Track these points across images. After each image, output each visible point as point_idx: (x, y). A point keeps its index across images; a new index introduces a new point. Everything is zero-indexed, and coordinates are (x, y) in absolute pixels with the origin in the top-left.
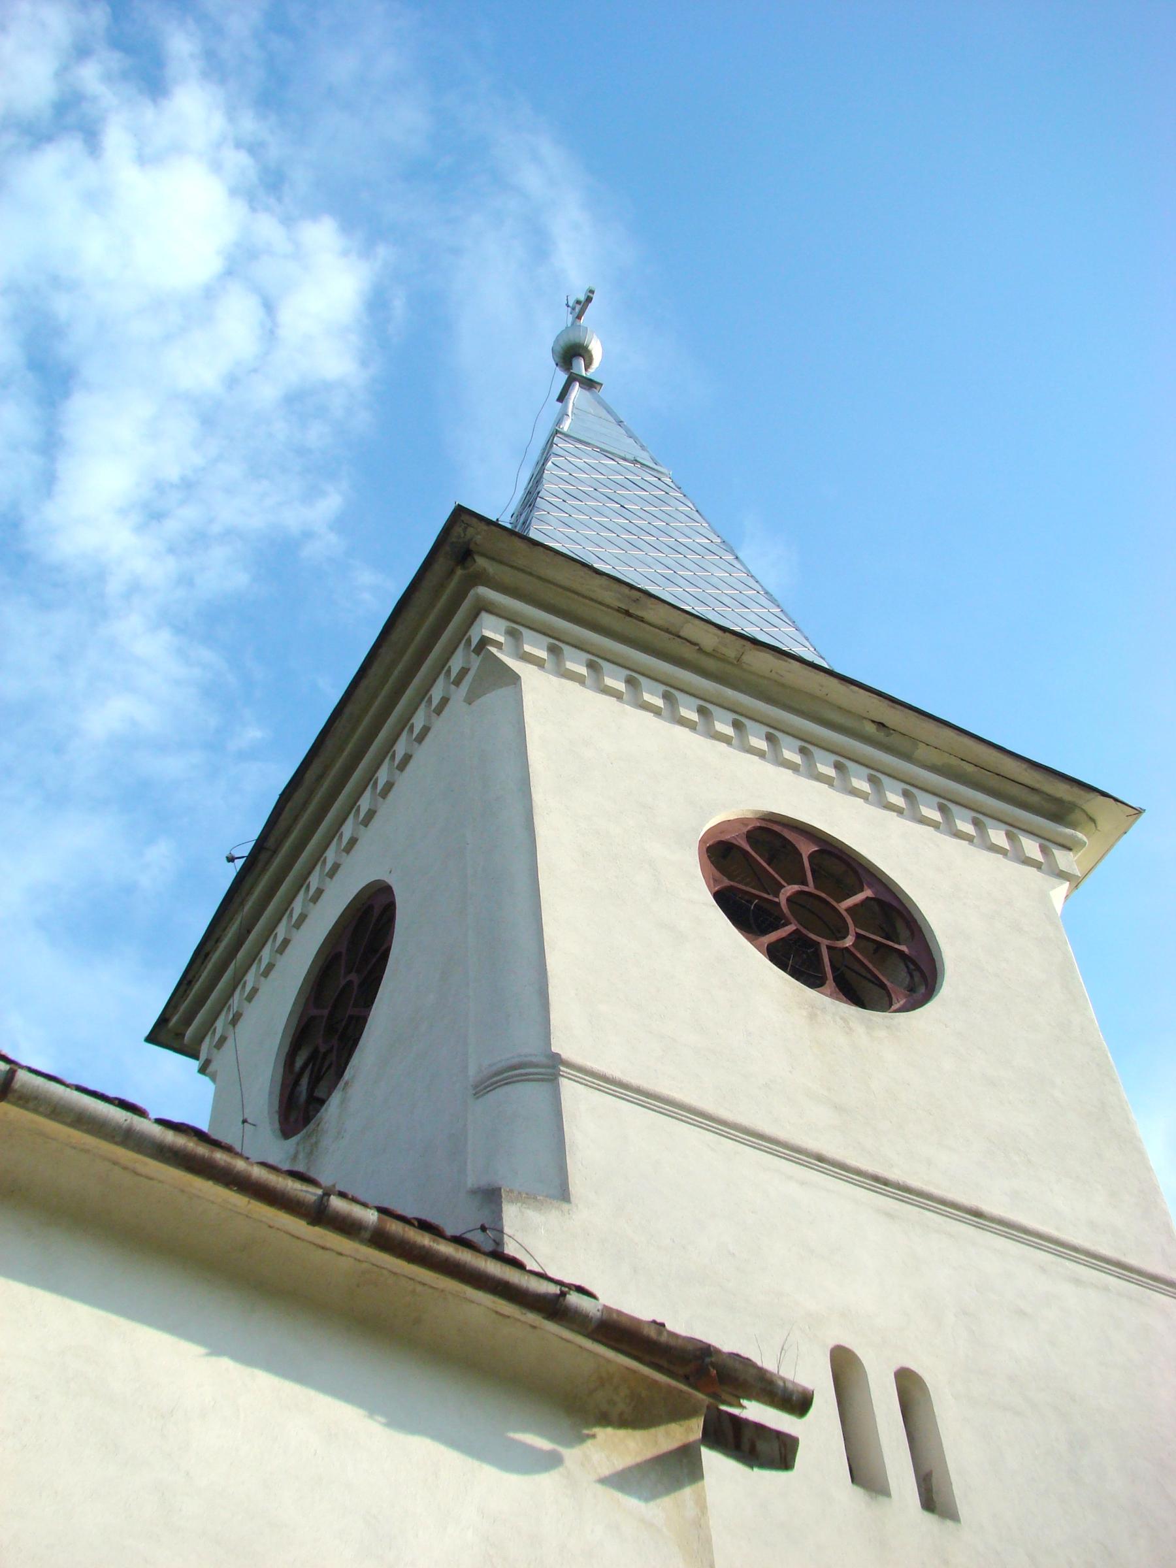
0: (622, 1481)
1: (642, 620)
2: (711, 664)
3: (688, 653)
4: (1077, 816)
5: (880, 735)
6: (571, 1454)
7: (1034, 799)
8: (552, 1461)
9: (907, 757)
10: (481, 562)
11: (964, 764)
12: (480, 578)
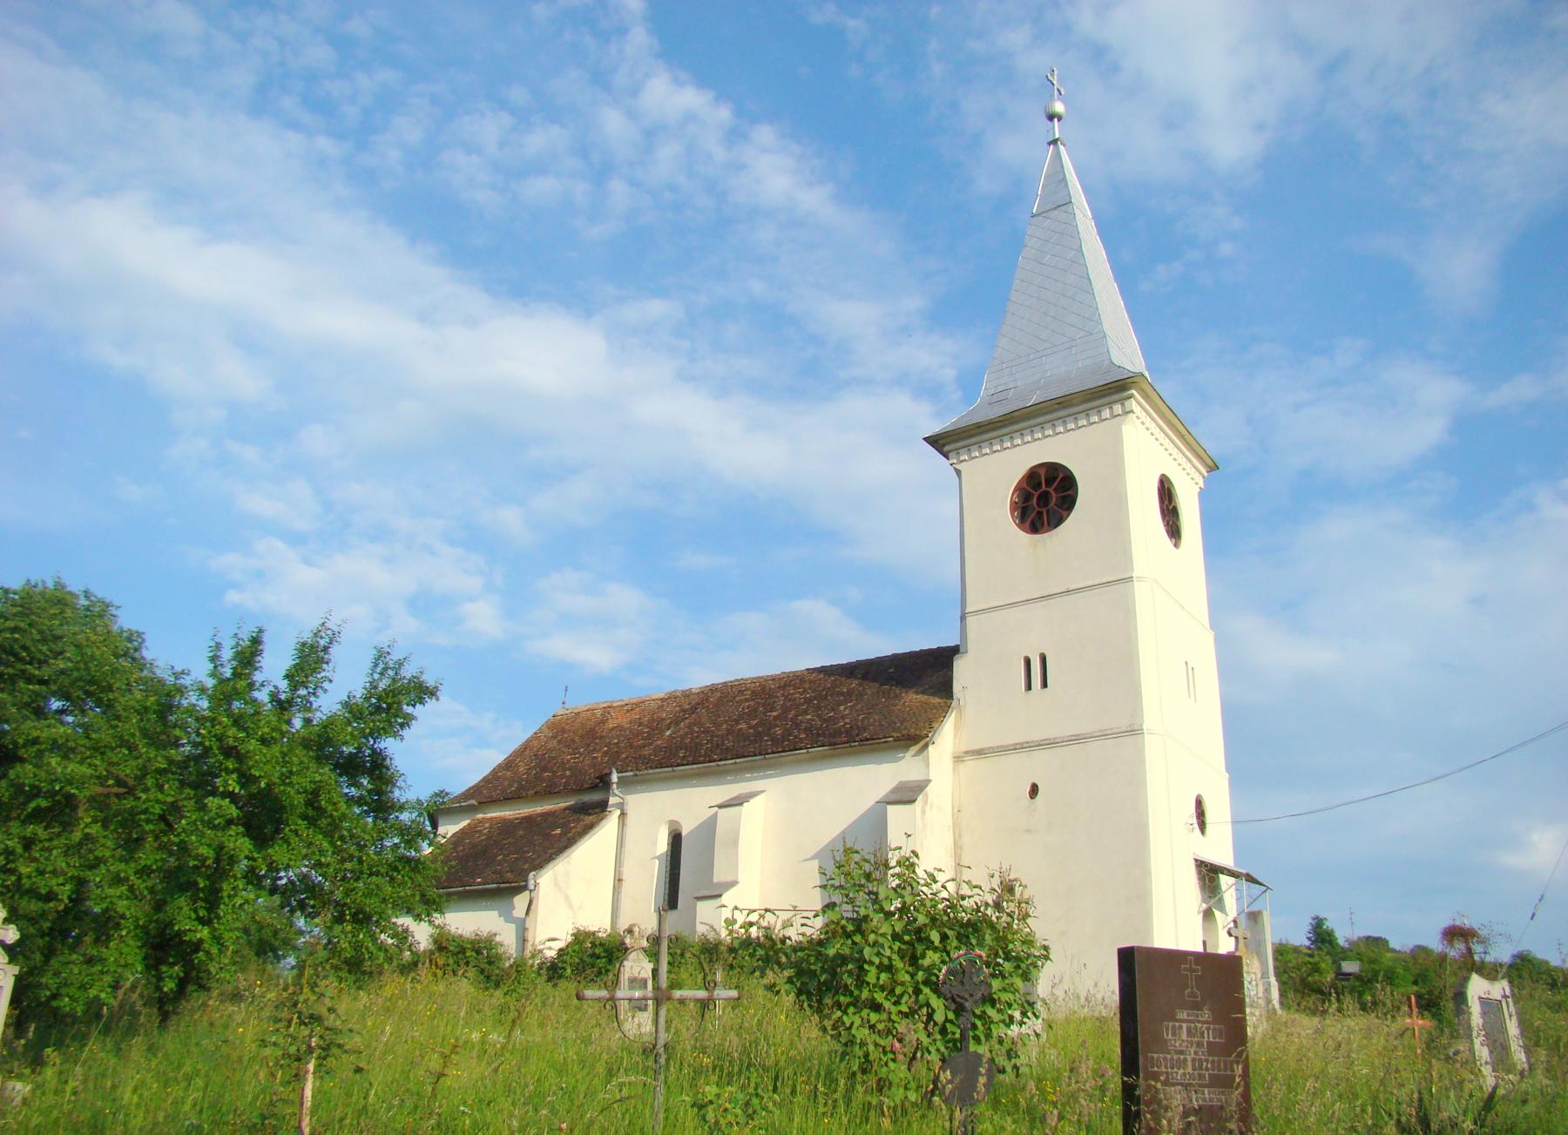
0: (914, 756)
3: (999, 424)
9: (1072, 406)
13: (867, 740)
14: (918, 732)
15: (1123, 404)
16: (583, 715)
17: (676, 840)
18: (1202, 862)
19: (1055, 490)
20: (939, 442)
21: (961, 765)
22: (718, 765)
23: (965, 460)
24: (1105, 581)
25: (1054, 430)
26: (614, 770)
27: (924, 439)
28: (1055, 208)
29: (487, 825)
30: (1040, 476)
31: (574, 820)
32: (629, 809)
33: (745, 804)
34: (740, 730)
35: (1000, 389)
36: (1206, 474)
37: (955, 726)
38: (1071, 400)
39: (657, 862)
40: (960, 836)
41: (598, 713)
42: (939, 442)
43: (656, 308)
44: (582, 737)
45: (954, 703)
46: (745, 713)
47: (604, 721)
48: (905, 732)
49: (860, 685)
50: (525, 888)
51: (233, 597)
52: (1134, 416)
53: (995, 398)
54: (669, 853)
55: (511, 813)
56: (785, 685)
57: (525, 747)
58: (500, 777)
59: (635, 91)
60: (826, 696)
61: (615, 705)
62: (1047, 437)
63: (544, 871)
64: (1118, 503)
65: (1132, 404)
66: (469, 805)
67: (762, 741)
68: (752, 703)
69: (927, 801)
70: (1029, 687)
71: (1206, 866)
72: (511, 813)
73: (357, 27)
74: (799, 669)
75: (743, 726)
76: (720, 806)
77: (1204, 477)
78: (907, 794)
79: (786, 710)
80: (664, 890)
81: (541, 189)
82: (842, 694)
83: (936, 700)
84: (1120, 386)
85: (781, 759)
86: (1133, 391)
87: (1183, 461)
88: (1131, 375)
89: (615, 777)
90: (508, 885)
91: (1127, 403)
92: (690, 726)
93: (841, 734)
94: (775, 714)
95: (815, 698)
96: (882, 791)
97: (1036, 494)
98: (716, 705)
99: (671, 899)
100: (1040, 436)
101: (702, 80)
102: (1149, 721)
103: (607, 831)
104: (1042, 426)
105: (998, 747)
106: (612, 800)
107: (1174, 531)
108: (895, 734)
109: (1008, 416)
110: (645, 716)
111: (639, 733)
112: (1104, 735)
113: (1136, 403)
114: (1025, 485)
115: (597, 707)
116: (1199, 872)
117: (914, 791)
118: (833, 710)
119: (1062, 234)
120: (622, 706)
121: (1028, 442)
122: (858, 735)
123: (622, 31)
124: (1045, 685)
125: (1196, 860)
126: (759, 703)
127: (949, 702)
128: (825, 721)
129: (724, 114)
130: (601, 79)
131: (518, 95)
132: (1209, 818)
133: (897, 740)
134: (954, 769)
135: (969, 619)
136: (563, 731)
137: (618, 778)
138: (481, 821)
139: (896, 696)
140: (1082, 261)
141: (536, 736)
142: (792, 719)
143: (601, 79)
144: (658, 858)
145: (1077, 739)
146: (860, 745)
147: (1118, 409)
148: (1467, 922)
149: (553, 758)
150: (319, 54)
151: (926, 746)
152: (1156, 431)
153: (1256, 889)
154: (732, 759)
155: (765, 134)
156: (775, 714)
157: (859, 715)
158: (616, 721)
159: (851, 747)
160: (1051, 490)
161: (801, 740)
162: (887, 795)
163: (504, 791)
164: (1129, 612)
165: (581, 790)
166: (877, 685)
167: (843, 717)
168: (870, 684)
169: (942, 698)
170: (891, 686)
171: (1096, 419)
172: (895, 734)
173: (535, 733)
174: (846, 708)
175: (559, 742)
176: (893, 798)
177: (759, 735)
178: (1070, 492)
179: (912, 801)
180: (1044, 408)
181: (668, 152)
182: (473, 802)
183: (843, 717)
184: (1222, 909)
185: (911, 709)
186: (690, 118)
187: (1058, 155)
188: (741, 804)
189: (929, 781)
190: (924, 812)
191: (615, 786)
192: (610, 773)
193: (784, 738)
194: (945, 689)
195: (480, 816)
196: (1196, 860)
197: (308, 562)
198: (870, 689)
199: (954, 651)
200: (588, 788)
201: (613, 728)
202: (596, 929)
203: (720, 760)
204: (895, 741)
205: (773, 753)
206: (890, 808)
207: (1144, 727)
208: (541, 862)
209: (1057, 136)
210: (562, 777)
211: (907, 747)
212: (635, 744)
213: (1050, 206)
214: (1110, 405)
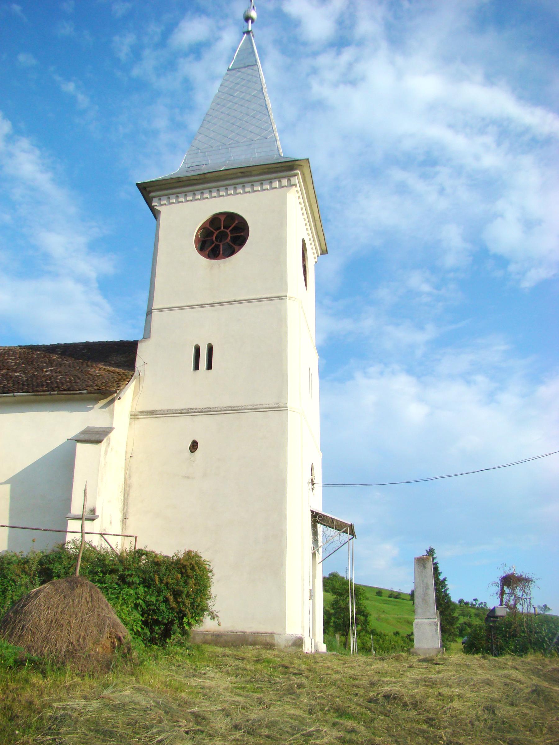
0: (102, 407)
1: (183, 181)
2: (201, 181)
3: (195, 182)
4: (295, 167)
5: (243, 175)
6: (95, 406)
7: (284, 169)
8: (93, 408)
9: (251, 176)
10: (148, 189)
11: (265, 170)
12: (150, 192)
13: (65, 390)
15: (289, 180)
19: (230, 231)
21: (136, 422)
28: (245, 67)
35: (195, 164)
38: (251, 172)
40: (130, 477)
48: (96, 388)
49: (60, 358)
60: (32, 362)
65: (294, 180)
70: (196, 367)
71: (320, 516)
74: (14, 345)
82: (45, 362)
84: (290, 166)
86: (298, 172)
93: (42, 386)
95: (23, 363)
96: (73, 432)
97: (216, 233)
104: (226, 187)
105: (168, 410)
109: (202, 177)
112: (255, 409)
118: (37, 371)
124: (209, 367)
125: (312, 512)
127: (132, 373)
134: (130, 424)
135: (154, 315)
139: (88, 366)
140: (262, 97)
145: (233, 410)
146: (58, 394)
147: (285, 182)
148: (518, 571)
151: (113, 401)
155: (25, 143)
159: (50, 394)
160: (228, 231)
161: (9, 387)
162: (77, 435)
164: (282, 321)
168: (68, 358)
170: (84, 360)
171: (259, 188)
174: (47, 371)
176: (82, 437)
178: (242, 234)
179: (99, 442)
183: (45, 376)
185: (101, 375)
190: (106, 452)
196: (312, 512)
198: (68, 361)
206: (79, 446)
209: (250, 29)
211: (96, 400)
214: (279, 179)
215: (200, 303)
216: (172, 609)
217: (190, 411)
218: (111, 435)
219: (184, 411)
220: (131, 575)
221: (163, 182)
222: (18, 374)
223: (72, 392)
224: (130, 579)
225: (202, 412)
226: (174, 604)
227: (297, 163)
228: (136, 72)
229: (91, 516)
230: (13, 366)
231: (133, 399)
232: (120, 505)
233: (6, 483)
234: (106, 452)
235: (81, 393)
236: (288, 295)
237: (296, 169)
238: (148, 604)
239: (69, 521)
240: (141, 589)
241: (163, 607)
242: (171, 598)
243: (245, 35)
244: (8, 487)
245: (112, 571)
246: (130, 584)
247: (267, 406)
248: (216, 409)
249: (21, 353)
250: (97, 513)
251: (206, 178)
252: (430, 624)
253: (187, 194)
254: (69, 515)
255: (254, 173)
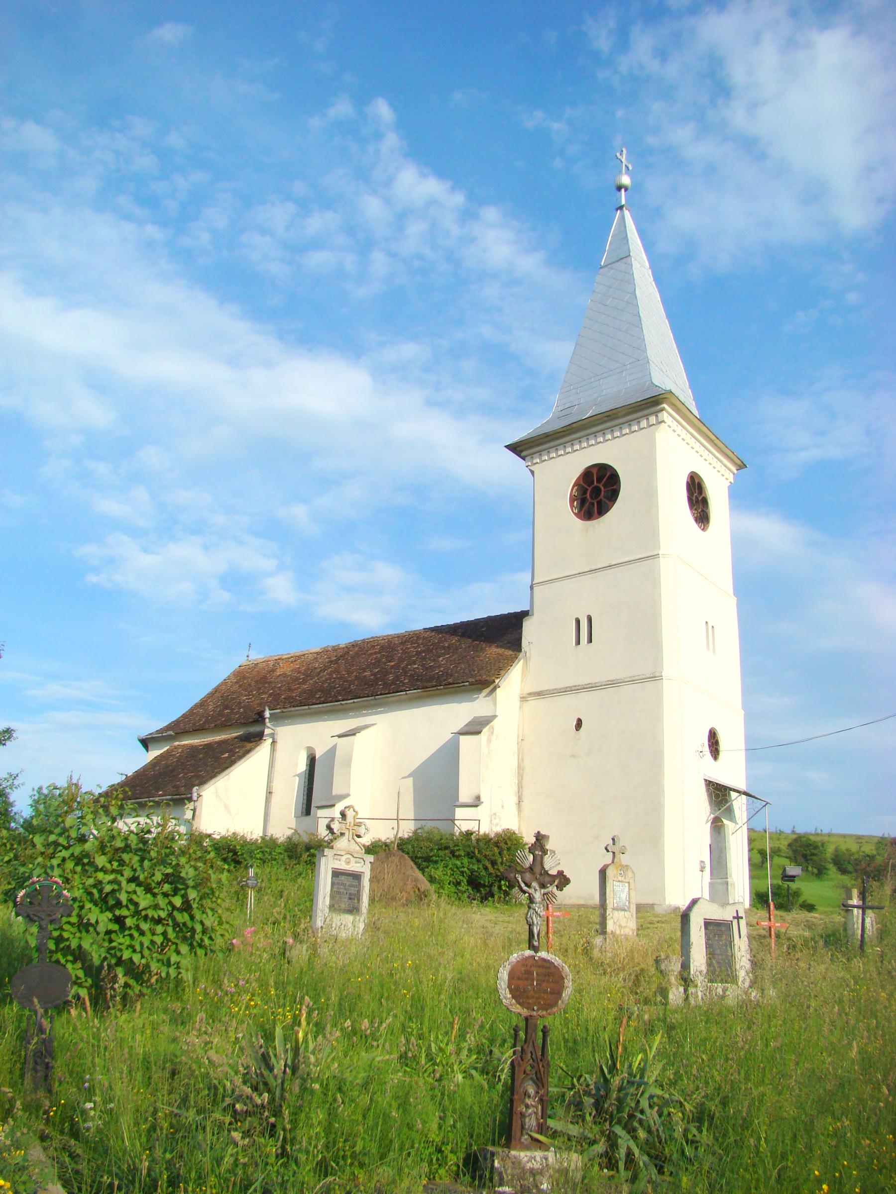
0: (485, 697)
9: (617, 418)
13: (450, 684)
14: (488, 678)
15: (657, 416)
16: (260, 665)
17: (312, 761)
18: (710, 782)
20: (517, 448)
21: (525, 704)
22: (341, 704)
23: (537, 463)
24: (637, 557)
25: (604, 438)
26: (267, 708)
27: (506, 446)
28: (618, 261)
29: (180, 750)
30: (593, 474)
31: (239, 747)
32: (279, 738)
33: (357, 734)
34: (365, 676)
36: (735, 471)
37: (522, 673)
39: (297, 778)
41: (271, 663)
42: (517, 448)
43: (409, 350)
44: (256, 682)
45: (521, 655)
46: (371, 664)
47: (274, 670)
48: (478, 678)
50: (190, 799)
51: (93, 578)
52: (666, 425)
53: (564, 413)
54: (307, 772)
55: (199, 741)
56: (405, 642)
57: (216, 690)
58: (194, 714)
59: (389, 183)
61: (284, 657)
62: (599, 443)
63: (206, 786)
64: (650, 494)
65: (664, 416)
66: (169, 735)
67: (377, 684)
68: (379, 655)
69: (492, 733)
70: (578, 642)
71: (713, 785)
72: (199, 741)
73: (174, 140)
75: (368, 673)
76: (340, 736)
77: (734, 474)
78: (474, 728)
79: (401, 660)
80: (302, 800)
81: (319, 260)
83: (509, 653)
85: (385, 700)
87: (714, 461)
88: (663, 392)
89: (267, 714)
90: (178, 797)
91: (660, 415)
92: (330, 674)
94: (393, 664)
96: (460, 724)
97: (590, 489)
98: (353, 658)
99: (307, 808)
100: (602, 440)
101: (441, 173)
102: (668, 671)
103: (262, 752)
105: (553, 690)
106: (267, 731)
107: (702, 517)
108: (470, 680)
109: (568, 428)
110: (303, 666)
111: (297, 679)
112: (633, 681)
113: (667, 414)
114: (582, 482)
115: (271, 659)
116: (708, 790)
117: (482, 724)
118: (434, 660)
119: (622, 281)
120: (289, 658)
121: (593, 445)
122: (445, 680)
123: (379, 136)
124: (590, 640)
125: (706, 780)
126: (384, 655)
127: (518, 653)
128: (427, 669)
129: (459, 199)
130: (363, 175)
131: (300, 188)
132: (722, 746)
133: (471, 684)
134: (521, 707)
136: (244, 678)
137: (271, 714)
138: (176, 747)
141: (224, 683)
142: (403, 669)
143: (363, 175)
144: (298, 775)
146: (444, 688)
147: (653, 419)
149: (234, 699)
150: (146, 162)
151: (494, 689)
152: (688, 437)
153: (759, 804)
154: (351, 699)
155: (491, 214)
156: (393, 664)
157: (451, 665)
158: (282, 670)
159: (437, 689)
160: (601, 486)
163: (194, 724)
164: (655, 582)
165: (246, 724)
166: (470, 641)
167: (439, 666)
169: (513, 651)
171: (627, 431)
172: (470, 680)
173: (225, 680)
175: (240, 686)
176: (468, 729)
177: (376, 680)
178: (615, 487)
179: (478, 733)
180: (591, 422)
181: (415, 229)
182: (171, 733)
184: (732, 819)
186: (432, 202)
187: (623, 219)
188: (354, 734)
189: (495, 717)
190: (489, 741)
191: (267, 720)
192: (264, 711)
193: (393, 683)
194: (516, 645)
195: (177, 743)
196: (706, 780)
197: (146, 550)
198: (466, 643)
199: (525, 614)
200: (252, 722)
201: (280, 675)
202: (212, 832)
203: (343, 700)
204: (470, 685)
205: (381, 694)
206: (462, 738)
207: (663, 674)
208: (203, 781)
210: (236, 713)
212: (293, 687)
213: (615, 259)
214: (646, 417)
215: (577, 572)
216: (491, 874)
217: (573, 688)
218: (495, 723)
219: (568, 689)
220: (459, 850)
221: (531, 440)
222: (416, 666)
223: (456, 685)
224: (457, 853)
225: (584, 688)
226: (491, 870)
227: (661, 396)
228: (625, 63)
229: (476, 802)
230: (414, 656)
231: (522, 681)
232: (515, 788)
233: (409, 776)
234: (489, 741)
235: (464, 686)
236: (660, 553)
237: (662, 403)
238: (472, 871)
239: (457, 809)
240: (466, 861)
241: (483, 873)
242: (489, 866)
243: (619, 211)
244: (411, 779)
245: (446, 848)
246: (458, 857)
247: (644, 677)
248: (597, 685)
249: (424, 638)
250: (482, 799)
251: (573, 428)
252: (722, 884)
253: (558, 447)
254: (457, 803)
255: (620, 414)
